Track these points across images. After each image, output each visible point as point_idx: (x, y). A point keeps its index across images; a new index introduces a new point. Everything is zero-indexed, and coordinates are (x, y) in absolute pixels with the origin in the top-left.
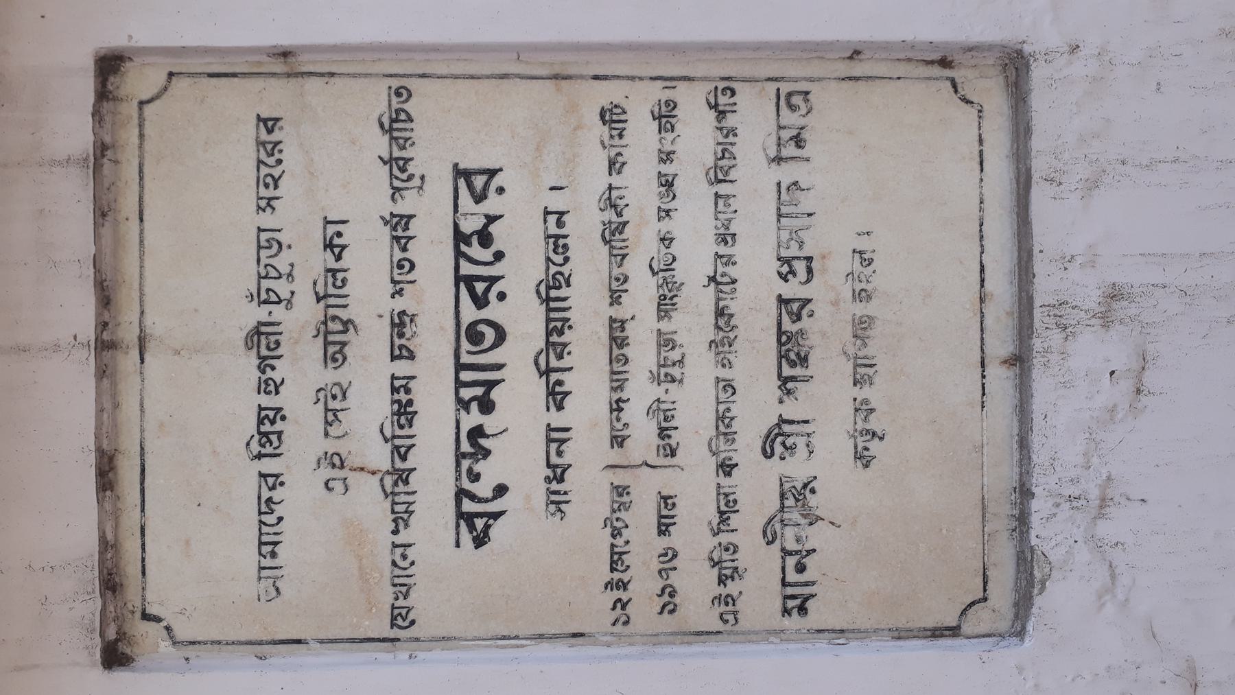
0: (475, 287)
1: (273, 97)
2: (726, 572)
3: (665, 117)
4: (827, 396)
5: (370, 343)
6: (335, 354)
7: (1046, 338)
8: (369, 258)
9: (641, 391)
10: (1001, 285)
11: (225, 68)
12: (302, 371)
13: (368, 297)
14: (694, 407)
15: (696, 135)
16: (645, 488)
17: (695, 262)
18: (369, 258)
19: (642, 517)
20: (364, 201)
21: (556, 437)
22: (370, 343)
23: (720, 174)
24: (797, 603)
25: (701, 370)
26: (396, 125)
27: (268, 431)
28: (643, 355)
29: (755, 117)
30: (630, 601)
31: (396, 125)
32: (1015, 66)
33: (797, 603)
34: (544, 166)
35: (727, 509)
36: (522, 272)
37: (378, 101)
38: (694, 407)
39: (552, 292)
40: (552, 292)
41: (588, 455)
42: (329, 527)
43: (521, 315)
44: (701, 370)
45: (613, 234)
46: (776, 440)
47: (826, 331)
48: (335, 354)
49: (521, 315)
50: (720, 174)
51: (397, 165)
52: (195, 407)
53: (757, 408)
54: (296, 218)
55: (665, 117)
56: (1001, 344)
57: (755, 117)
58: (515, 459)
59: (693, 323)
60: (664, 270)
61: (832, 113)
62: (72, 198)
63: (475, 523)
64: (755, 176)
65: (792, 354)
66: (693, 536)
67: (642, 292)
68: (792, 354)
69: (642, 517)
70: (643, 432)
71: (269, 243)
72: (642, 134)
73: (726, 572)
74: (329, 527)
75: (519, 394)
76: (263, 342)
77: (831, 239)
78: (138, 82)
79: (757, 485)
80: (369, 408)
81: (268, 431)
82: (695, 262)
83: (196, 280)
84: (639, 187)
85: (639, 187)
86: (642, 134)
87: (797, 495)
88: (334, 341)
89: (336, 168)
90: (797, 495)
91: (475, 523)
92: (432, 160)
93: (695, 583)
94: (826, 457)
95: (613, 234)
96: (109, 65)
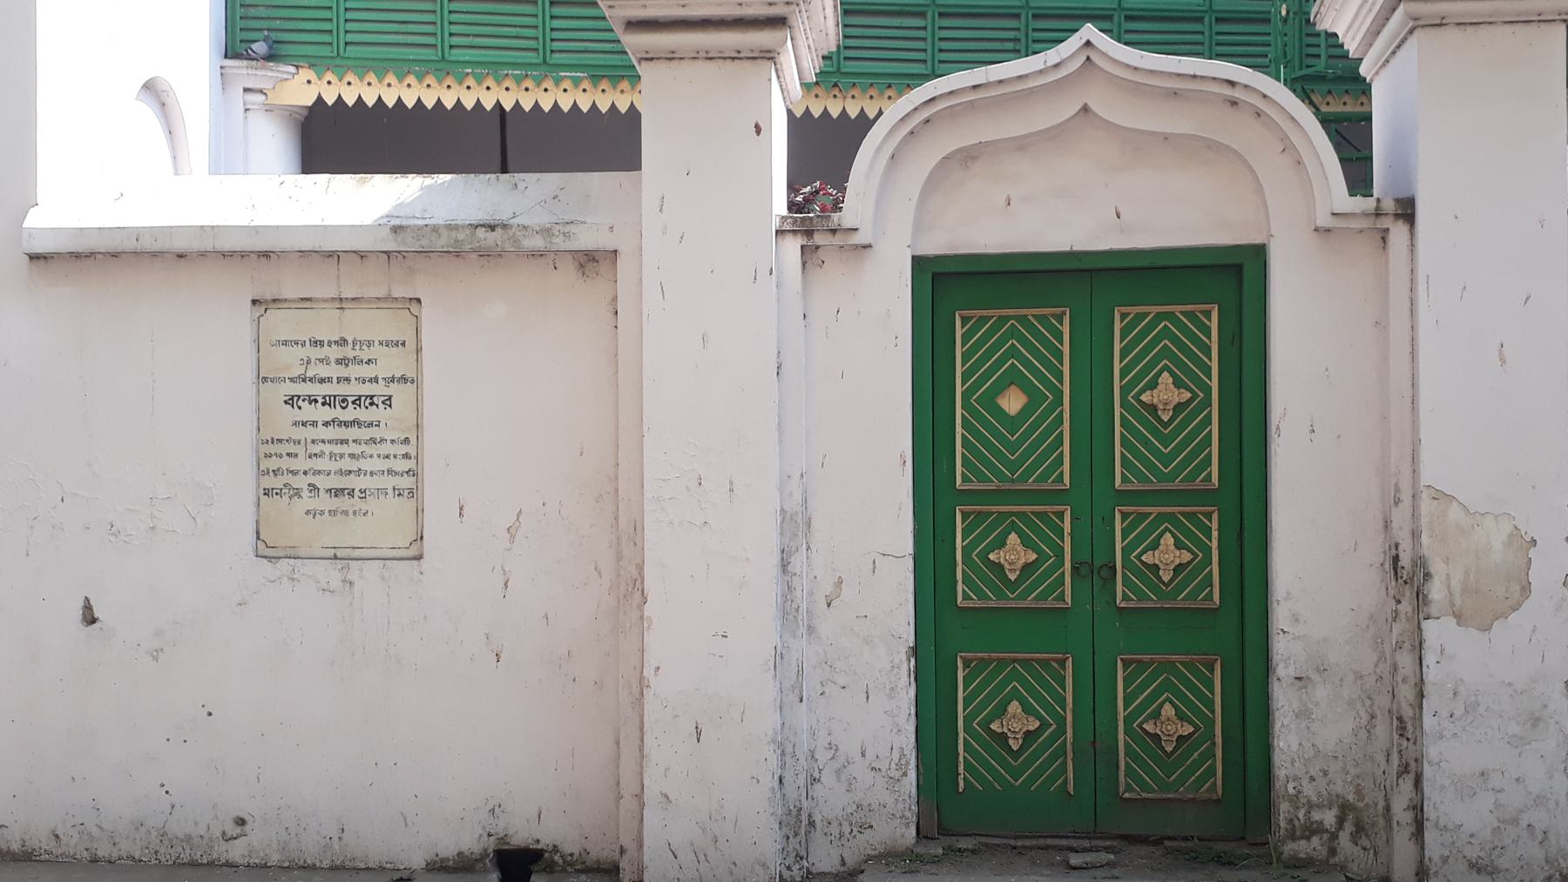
0: (357, 401)
1: (411, 345)
3: (406, 456)
4: (325, 502)
5: (342, 371)
6: (339, 362)
7: (340, 564)
9: (327, 448)
10: (357, 553)
12: (334, 353)
13: (354, 371)
14: (323, 464)
19: (292, 449)
20: (382, 369)
21: (314, 424)
22: (342, 371)
25: (334, 466)
26: (403, 379)
27: (317, 343)
28: (338, 449)
29: (406, 482)
30: (268, 445)
32: (419, 557)
34: (391, 421)
35: (294, 473)
36: (363, 414)
37: (410, 374)
38: (323, 464)
41: (310, 433)
42: (290, 360)
43: (350, 414)
44: (334, 466)
45: (373, 441)
46: (313, 488)
47: (344, 502)
48: (339, 362)
49: (350, 414)
51: (393, 379)
52: (325, 324)
53: (323, 482)
54: (376, 351)
55: (406, 456)
56: (339, 553)
57: (406, 482)
58: (308, 412)
59: (347, 464)
60: (363, 455)
62: (382, 293)
63: (291, 401)
64: (389, 482)
66: (286, 463)
67: (356, 449)
68: (338, 492)
69: (292, 449)
70: (316, 449)
71: (370, 344)
72: (403, 449)
75: (326, 413)
76: (342, 342)
77: (371, 504)
78: (414, 308)
79: (301, 482)
80: (323, 371)
81: (317, 343)
82: (365, 464)
83: (362, 324)
84: (387, 448)
85: (387, 448)
86: (403, 449)
87: (297, 493)
89: (390, 363)
90: (297, 493)
91: (291, 401)
92: (394, 389)
93: (272, 464)
94: (307, 502)
95: (373, 441)
96: (419, 300)
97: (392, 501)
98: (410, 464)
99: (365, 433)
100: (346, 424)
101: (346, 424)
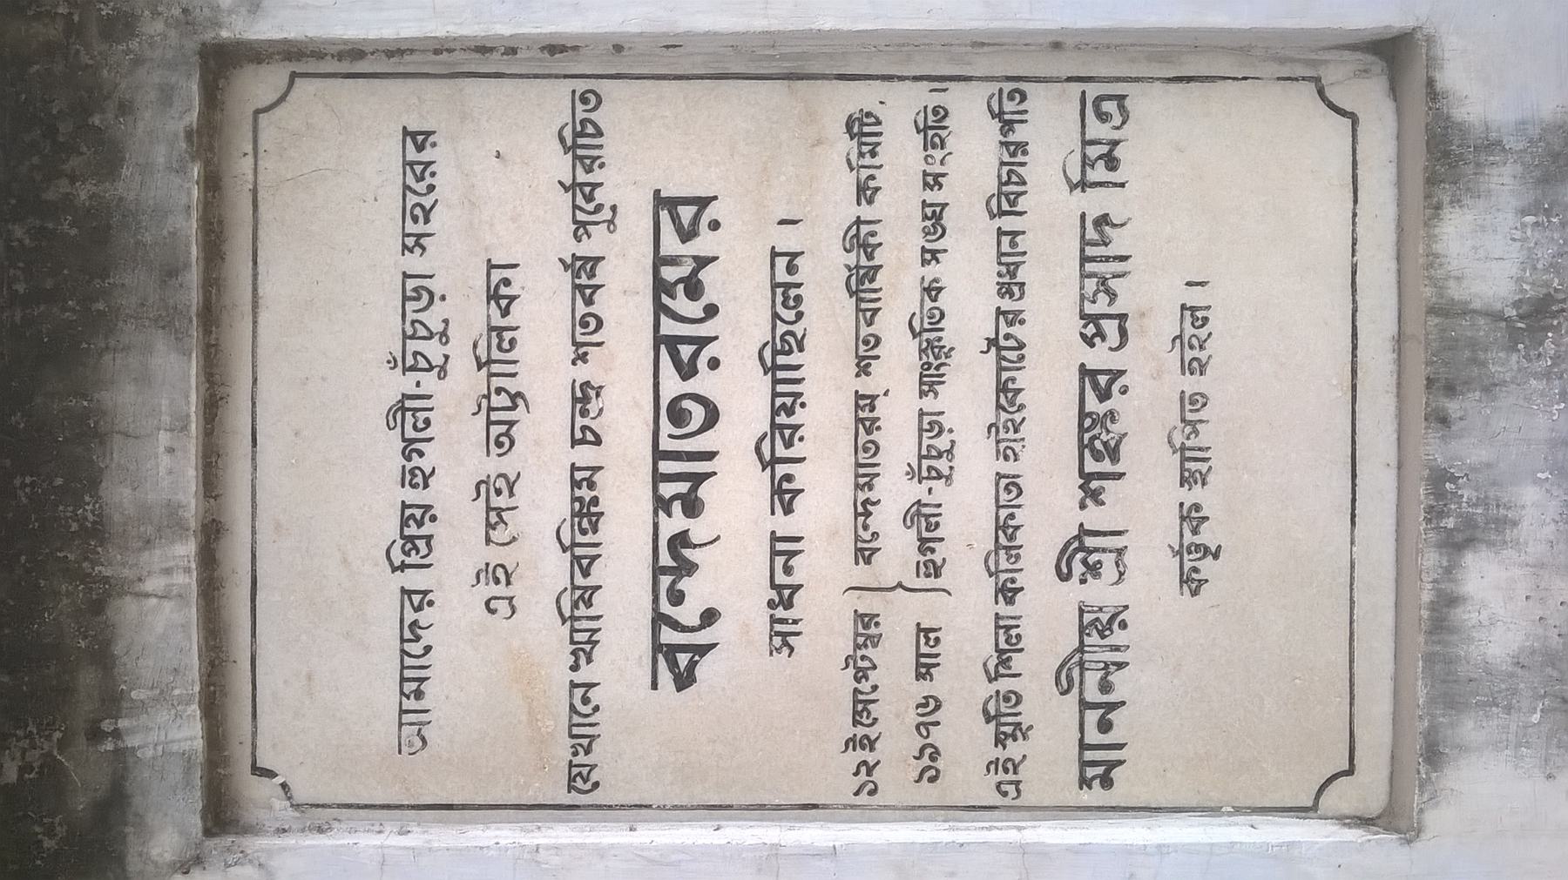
1: (423, 103)
2: (1004, 721)
3: (933, 129)
4: (1145, 501)
8: (543, 311)
9: (896, 491)
11: (354, 61)
12: (457, 455)
13: (544, 367)
15: (974, 151)
16: (899, 621)
17: (970, 313)
18: (543, 311)
20: (538, 238)
21: (783, 549)
23: (1006, 199)
24: (1098, 769)
25: (975, 464)
26: (581, 142)
27: (414, 534)
29: (1052, 128)
31: (581, 142)
33: (1098, 769)
39: (780, 358)
40: (780, 358)
41: (825, 571)
43: (741, 394)
45: (862, 282)
46: (1079, 555)
47: (1144, 413)
49: (741, 394)
50: (1006, 199)
51: (581, 192)
53: (1050, 513)
54: (454, 266)
55: (933, 129)
57: (1052, 128)
58: (729, 578)
61: (1160, 126)
63: (678, 661)
64: (1051, 209)
65: (1098, 445)
66: (963, 684)
67: (899, 357)
68: (1098, 445)
70: (897, 545)
71: (417, 292)
72: (901, 151)
73: (1004, 721)
74: (494, 662)
75: (735, 494)
80: (543, 505)
81: (414, 534)
82: (970, 313)
86: (901, 151)
88: (500, 422)
90: (1098, 624)
91: (678, 661)
92: (626, 186)
93: (965, 738)
94: (1145, 584)
95: (862, 282)
97: (1149, 204)
98: (970, 115)
99: (827, 317)
100: (785, 406)
101: (785, 406)
